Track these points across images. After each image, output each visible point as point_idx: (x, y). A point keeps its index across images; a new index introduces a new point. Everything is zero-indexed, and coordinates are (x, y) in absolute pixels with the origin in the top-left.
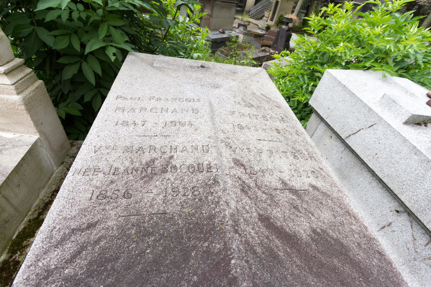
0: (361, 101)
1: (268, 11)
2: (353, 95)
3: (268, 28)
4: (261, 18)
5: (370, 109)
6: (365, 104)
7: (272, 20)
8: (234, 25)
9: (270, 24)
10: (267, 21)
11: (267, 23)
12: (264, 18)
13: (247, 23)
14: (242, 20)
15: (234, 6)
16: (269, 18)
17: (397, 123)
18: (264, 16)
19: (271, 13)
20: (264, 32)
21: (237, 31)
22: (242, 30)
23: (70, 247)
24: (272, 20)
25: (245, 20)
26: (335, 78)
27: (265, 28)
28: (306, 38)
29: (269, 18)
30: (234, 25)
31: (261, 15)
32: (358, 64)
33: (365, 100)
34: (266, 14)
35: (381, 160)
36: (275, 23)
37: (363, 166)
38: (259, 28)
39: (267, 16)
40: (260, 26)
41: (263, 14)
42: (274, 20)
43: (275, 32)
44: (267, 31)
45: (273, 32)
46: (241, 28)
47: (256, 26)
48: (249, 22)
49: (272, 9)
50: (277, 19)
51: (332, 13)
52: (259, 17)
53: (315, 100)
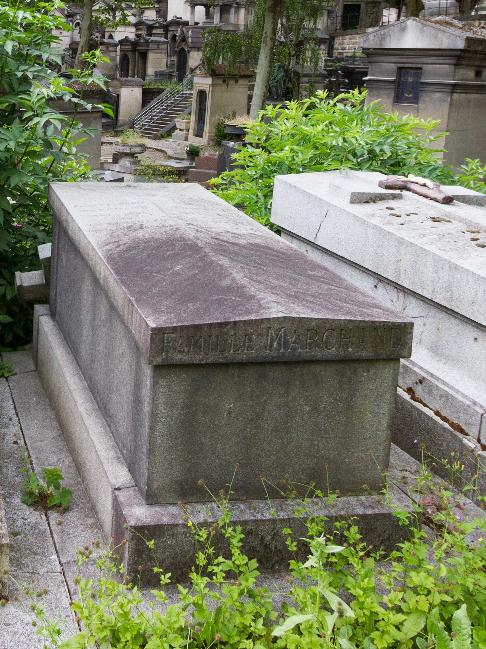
0: (312, 195)
1: (183, 115)
2: (304, 192)
3: (193, 153)
4: (169, 134)
5: (320, 199)
6: (315, 196)
7: (199, 133)
8: (102, 158)
9: (196, 144)
10: (186, 139)
11: (187, 143)
12: (177, 132)
13: (138, 149)
14: (124, 145)
15: (96, 118)
16: (191, 131)
17: (344, 203)
18: (174, 128)
19: (193, 118)
20: (185, 164)
21: (117, 168)
22: (128, 164)
23: (150, 192)
24: (199, 133)
25: (133, 144)
26: (285, 182)
27: (185, 156)
28: (249, 150)
29: (191, 131)
30: (102, 158)
31: (167, 128)
32: (315, 165)
33: (315, 194)
34: (180, 122)
35: (343, 242)
36: (210, 139)
37: (341, 263)
38: (170, 157)
39: (183, 127)
40: (170, 152)
41: (171, 124)
42: (206, 134)
43: (214, 159)
44: (192, 160)
45: (208, 159)
46: (126, 162)
47: (160, 154)
48: (142, 146)
49: (194, 108)
50: (214, 130)
51: (274, 115)
52: (162, 131)
53: (276, 214)
